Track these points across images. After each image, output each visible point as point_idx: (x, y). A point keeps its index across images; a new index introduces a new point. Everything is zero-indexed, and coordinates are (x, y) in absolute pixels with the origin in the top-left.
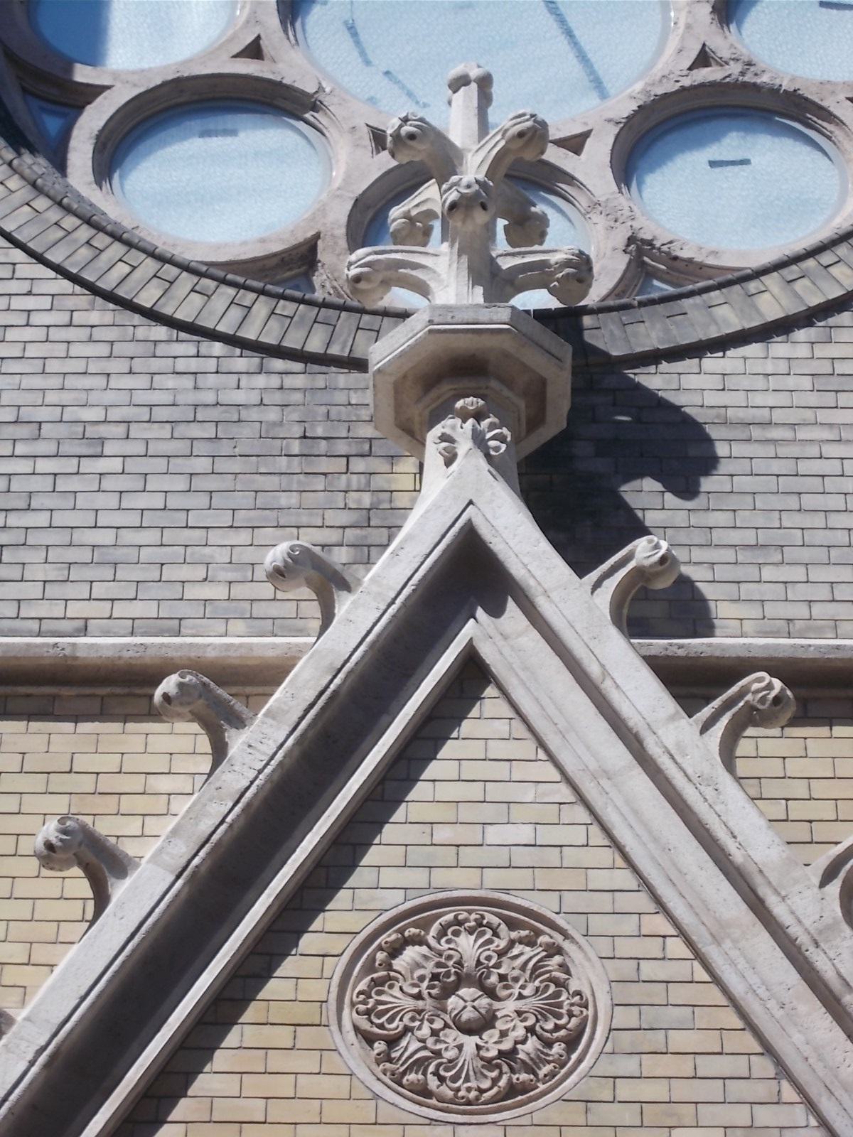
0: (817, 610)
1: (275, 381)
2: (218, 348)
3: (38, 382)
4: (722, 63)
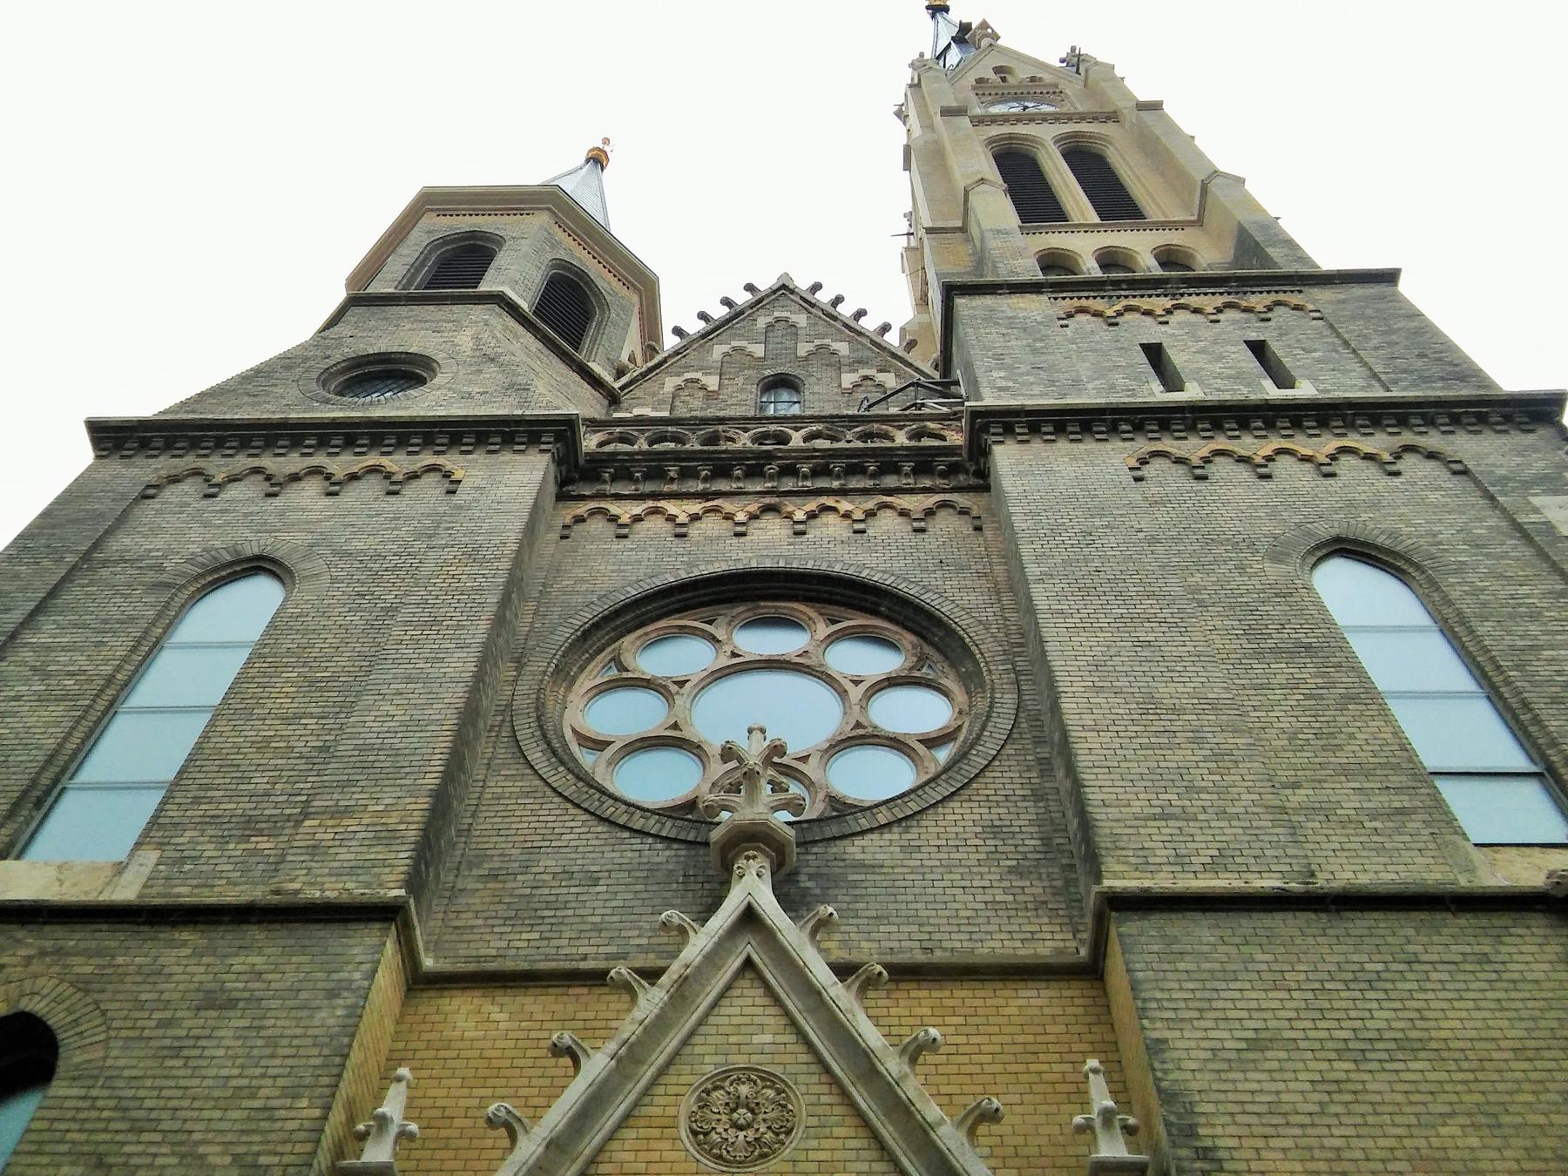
0: (903, 943)
1: (673, 853)
2: (650, 840)
3: (573, 856)
4: (864, 727)
